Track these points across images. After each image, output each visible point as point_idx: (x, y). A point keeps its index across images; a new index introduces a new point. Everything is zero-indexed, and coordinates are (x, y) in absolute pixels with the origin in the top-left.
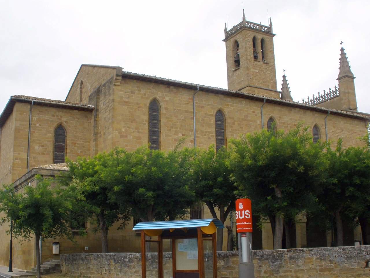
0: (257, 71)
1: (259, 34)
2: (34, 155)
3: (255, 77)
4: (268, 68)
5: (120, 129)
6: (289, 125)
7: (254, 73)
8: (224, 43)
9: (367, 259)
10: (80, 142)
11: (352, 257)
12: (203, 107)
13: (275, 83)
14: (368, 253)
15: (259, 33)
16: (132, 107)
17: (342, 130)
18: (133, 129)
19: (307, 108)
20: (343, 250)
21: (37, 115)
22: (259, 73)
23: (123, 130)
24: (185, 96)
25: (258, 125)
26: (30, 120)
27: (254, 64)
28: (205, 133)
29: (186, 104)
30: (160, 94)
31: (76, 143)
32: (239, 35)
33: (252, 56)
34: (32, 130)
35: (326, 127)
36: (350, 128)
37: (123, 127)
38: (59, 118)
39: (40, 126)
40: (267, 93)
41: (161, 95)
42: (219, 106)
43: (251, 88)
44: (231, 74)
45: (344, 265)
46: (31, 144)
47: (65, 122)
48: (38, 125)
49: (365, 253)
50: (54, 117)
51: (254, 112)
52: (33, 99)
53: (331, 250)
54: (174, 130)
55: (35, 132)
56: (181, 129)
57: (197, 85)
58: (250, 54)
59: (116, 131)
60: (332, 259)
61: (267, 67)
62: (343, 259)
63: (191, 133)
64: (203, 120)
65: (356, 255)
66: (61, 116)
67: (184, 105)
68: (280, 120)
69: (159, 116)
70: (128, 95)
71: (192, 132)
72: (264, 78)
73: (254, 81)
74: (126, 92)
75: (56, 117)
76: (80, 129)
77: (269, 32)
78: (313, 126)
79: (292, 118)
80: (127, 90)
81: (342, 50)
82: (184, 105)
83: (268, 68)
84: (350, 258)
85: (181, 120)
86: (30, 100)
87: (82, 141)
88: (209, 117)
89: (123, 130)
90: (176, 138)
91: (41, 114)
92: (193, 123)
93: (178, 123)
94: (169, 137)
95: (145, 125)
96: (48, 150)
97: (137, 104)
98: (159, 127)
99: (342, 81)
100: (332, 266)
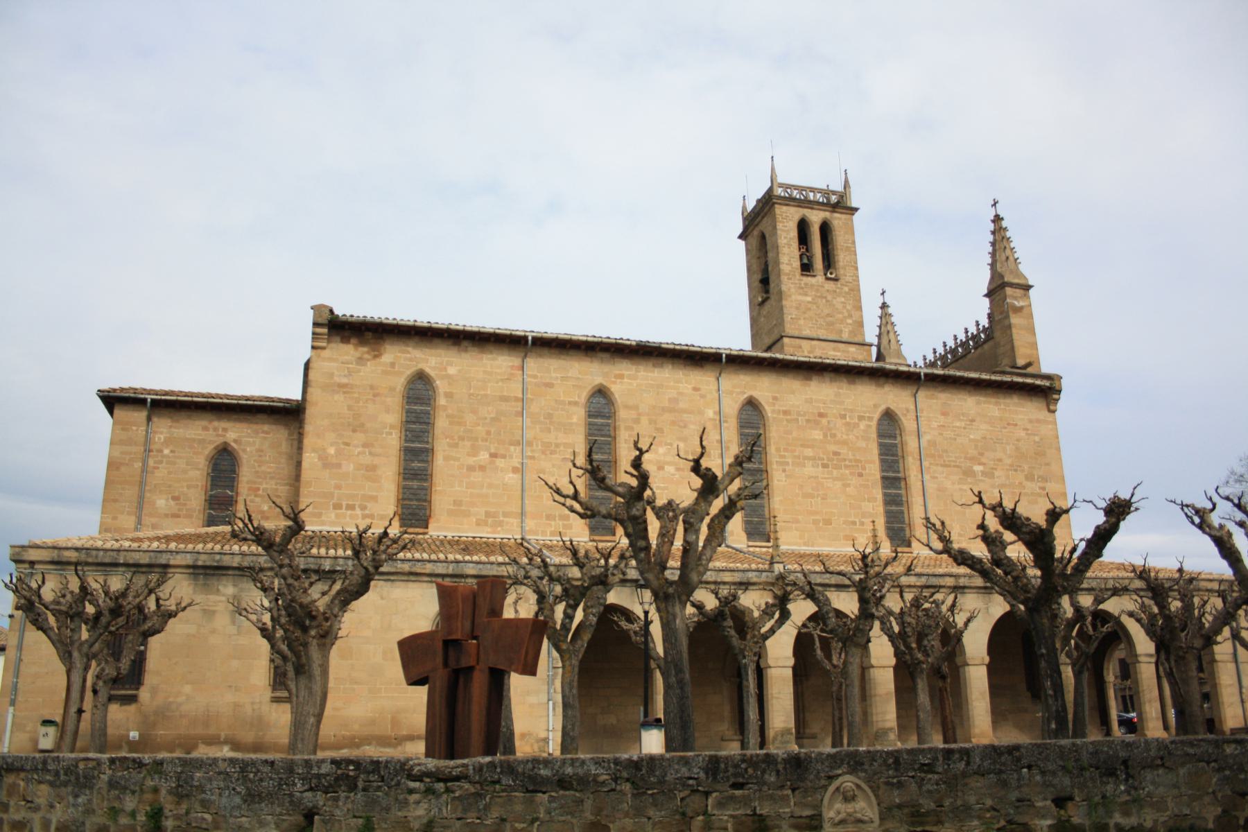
0: (809, 299)
1: (815, 212)
2: (154, 520)
3: (804, 313)
4: (838, 290)
5: (324, 450)
6: (801, 416)
7: (800, 304)
8: (742, 243)
9: (306, 806)
10: (268, 486)
11: (264, 795)
12: (550, 385)
13: (860, 324)
14: (313, 785)
15: (812, 208)
16: (356, 395)
17: (973, 421)
18: (356, 446)
19: (856, 371)
20: (240, 767)
21: (164, 428)
22: (815, 303)
23: (332, 451)
24: (501, 362)
25: (710, 419)
26: (147, 441)
27: (800, 284)
28: (553, 448)
29: (502, 380)
30: (432, 360)
31: (258, 489)
32: (765, 219)
33: (797, 264)
34: (151, 462)
35: (917, 416)
36: (997, 414)
37: (332, 445)
38: (220, 432)
39: (171, 455)
40: (834, 350)
41: (436, 363)
42: (598, 380)
43: (792, 339)
44: (755, 314)
45: (239, 820)
46: (148, 495)
47: (235, 441)
48: (166, 452)
49: (303, 784)
50: (208, 431)
51: (696, 389)
52: (149, 394)
53: (210, 765)
54: (468, 443)
55: (158, 468)
56: (486, 440)
57: (527, 334)
58: (790, 261)
59: (313, 455)
60: (208, 797)
61: (838, 288)
62: (237, 800)
63: (515, 449)
64: (550, 416)
65: (275, 787)
66: (225, 430)
67: (497, 383)
68: (774, 404)
69: (432, 412)
70: (348, 368)
71: (517, 448)
72: (828, 315)
73: (802, 322)
74: (343, 363)
75: (211, 432)
76: (270, 456)
77: (841, 204)
78: (877, 416)
79: (811, 399)
80: (346, 357)
81: (997, 219)
82: (497, 383)
83: (838, 290)
84: (257, 799)
85: (487, 421)
86: (142, 396)
87: (273, 482)
88: (567, 407)
89: (332, 451)
90: (472, 463)
91: (175, 428)
92: (520, 424)
93: (480, 428)
94: (452, 462)
95: (390, 437)
96: (188, 507)
97: (372, 387)
98: (430, 440)
99: (997, 299)
100: (204, 819)
